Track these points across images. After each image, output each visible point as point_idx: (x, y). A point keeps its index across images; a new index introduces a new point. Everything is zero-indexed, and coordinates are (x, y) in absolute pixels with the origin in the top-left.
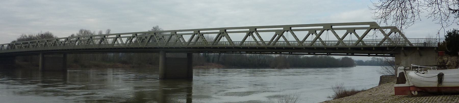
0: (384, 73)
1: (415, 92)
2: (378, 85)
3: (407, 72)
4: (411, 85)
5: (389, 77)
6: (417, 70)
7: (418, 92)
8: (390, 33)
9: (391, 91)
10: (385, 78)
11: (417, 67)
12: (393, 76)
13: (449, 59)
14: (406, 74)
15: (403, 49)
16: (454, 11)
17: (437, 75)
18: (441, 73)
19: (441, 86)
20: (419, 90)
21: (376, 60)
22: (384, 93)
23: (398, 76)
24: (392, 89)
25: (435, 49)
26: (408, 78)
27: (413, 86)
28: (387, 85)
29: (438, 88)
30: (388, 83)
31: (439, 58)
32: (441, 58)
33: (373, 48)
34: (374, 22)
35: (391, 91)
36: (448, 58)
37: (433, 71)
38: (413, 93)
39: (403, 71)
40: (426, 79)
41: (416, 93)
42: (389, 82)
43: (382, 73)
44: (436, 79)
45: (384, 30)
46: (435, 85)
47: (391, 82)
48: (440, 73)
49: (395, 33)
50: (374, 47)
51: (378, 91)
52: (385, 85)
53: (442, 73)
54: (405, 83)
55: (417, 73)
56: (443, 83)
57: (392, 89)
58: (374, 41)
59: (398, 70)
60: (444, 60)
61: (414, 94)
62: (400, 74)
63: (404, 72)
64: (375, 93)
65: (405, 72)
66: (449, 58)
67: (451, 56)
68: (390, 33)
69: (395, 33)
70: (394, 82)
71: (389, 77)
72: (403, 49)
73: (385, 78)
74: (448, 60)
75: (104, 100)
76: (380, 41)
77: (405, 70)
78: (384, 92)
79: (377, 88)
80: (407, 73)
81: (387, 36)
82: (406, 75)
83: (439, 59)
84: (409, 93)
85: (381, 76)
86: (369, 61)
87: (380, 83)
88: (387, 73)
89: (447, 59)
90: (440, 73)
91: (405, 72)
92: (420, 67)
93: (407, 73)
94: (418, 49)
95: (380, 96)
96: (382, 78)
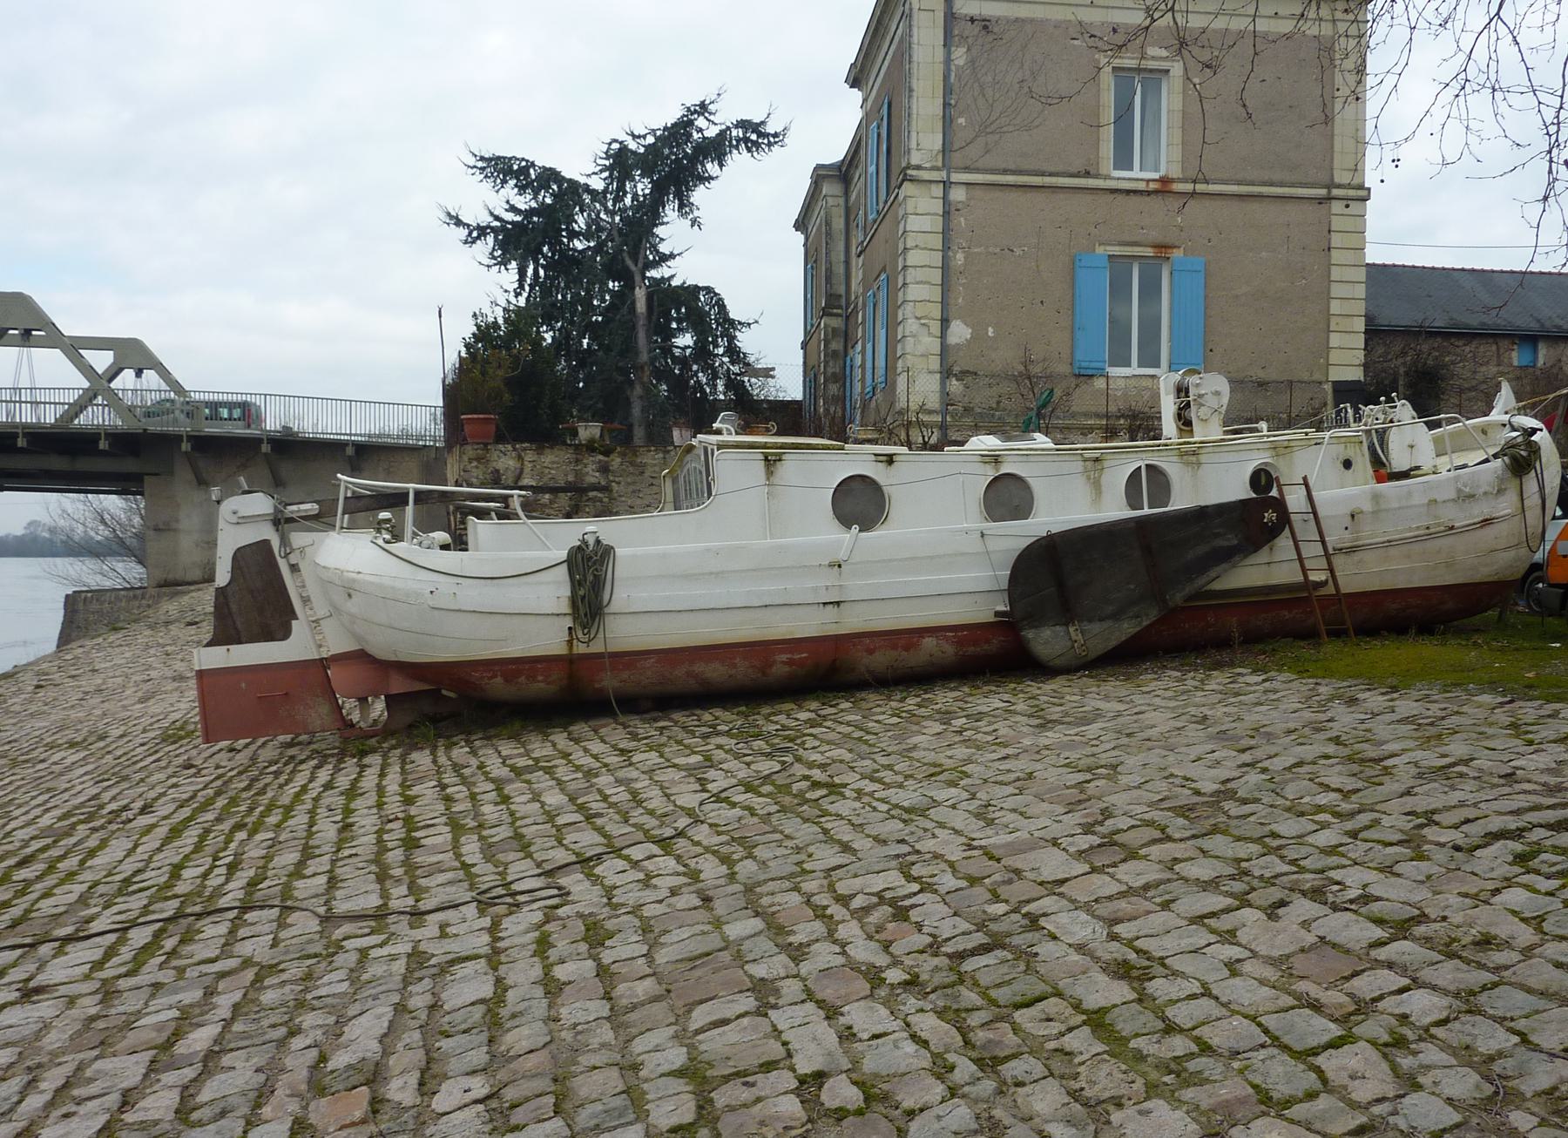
0: (84, 579)
1: (363, 700)
2: (51, 647)
3: (299, 539)
4: (337, 644)
5: (118, 599)
6: (388, 521)
7: (391, 701)
8: (114, 372)
9: (145, 687)
10: (95, 606)
11: (398, 500)
12: (138, 592)
13: (528, 466)
14: (293, 559)
15: (186, 446)
16: (470, 234)
17: (563, 555)
18: (591, 540)
19: (597, 647)
20: (399, 685)
21: (46, 535)
22: (98, 712)
23: (223, 577)
24: (153, 674)
25: (350, 451)
26: (313, 590)
27: (361, 657)
28: (111, 645)
29: (569, 663)
30: (115, 629)
31: (465, 458)
32: (478, 459)
33: (15, 435)
34: (20, 294)
35: (145, 687)
36: (520, 458)
37: (524, 527)
38: (350, 706)
39: (268, 533)
40: (475, 596)
41: (378, 708)
42: (120, 625)
43: (74, 582)
44: (554, 593)
45: (87, 354)
46: (549, 639)
47: (135, 626)
48: (584, 541)
49: (139, 373)
50: (25, 435)
51: (51, 693)
52: (99, 648)
53: (598, 541)
54: (284, 633)
55: (394, 547)
56: (608, 619)
57: (153, 674)
58: (21, 402)
59: (221, 524)
60: (497, 471)
61: (355, 717)
62: (240, 556)
63: (275, 544)
64: (33, 708)
65: (284, 541)
66: (529, 456)
67: (540, 451)
68: (114, 372)
69: (139, 373)
70: (151, 627)
71: (118, 599)
72: (186, 446)
73: (95, 606)
74: (522, 470)
75: (1398, 479)
76: (64, 404)
77: (280, 521)
78: (96, 700)
79: (44, 666)
80: (302, 550)
81: (99, 386)
82: (294, 568)
83: (470, 461)
84: (318, 713)
85: (67, 596)
86: (16, 537)
87: (65, 639)
88: (99, 578)
89: (519, 465)
90: (584, 541)
91: (284, 541)
92: (418, 493)
93: (302, 550)
94: (265, 448)
95: (72, 744)
96: (71, 602)
